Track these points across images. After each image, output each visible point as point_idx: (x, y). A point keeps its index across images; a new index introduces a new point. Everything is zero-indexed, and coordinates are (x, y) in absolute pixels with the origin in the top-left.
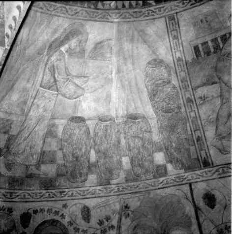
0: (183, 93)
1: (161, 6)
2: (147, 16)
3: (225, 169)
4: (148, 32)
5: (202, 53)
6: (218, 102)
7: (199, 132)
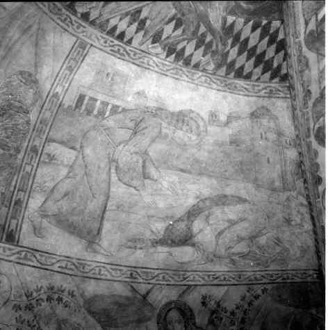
0: (33, 136)
1: (83, 24)
2: (61, 20)
3: (29, 255)
4: (48, 38)
5: (83, 107)
6: (64, 172)
7: (23, 193)
